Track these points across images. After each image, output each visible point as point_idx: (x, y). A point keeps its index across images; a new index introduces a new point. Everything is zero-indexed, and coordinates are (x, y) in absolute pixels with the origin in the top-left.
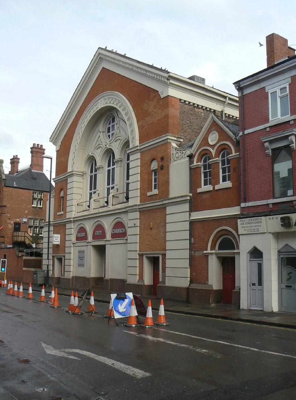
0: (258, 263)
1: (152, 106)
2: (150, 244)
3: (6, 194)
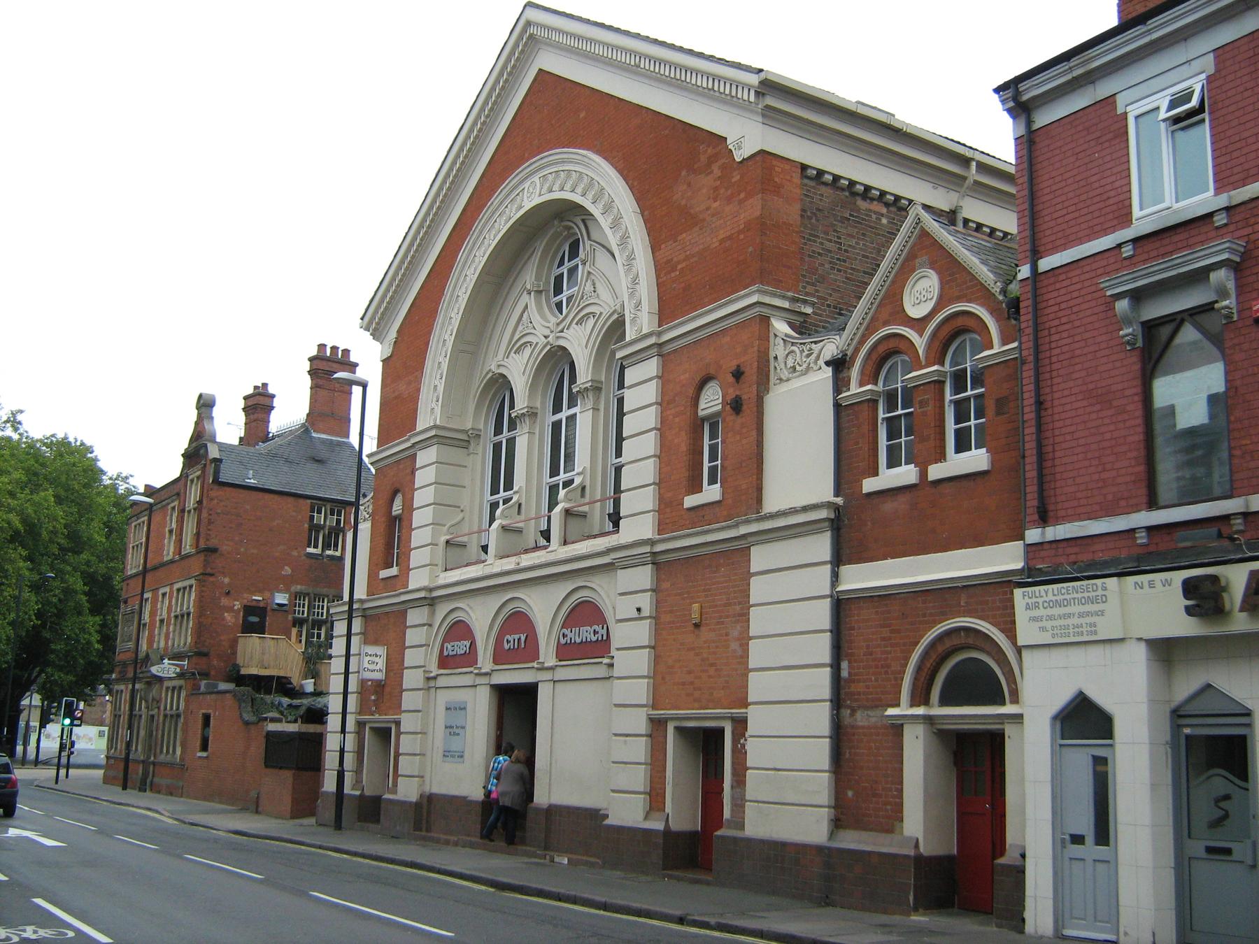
0: (1093, 756)
1: (704, 191)
2: (692, 683)
3: (219, 511)
